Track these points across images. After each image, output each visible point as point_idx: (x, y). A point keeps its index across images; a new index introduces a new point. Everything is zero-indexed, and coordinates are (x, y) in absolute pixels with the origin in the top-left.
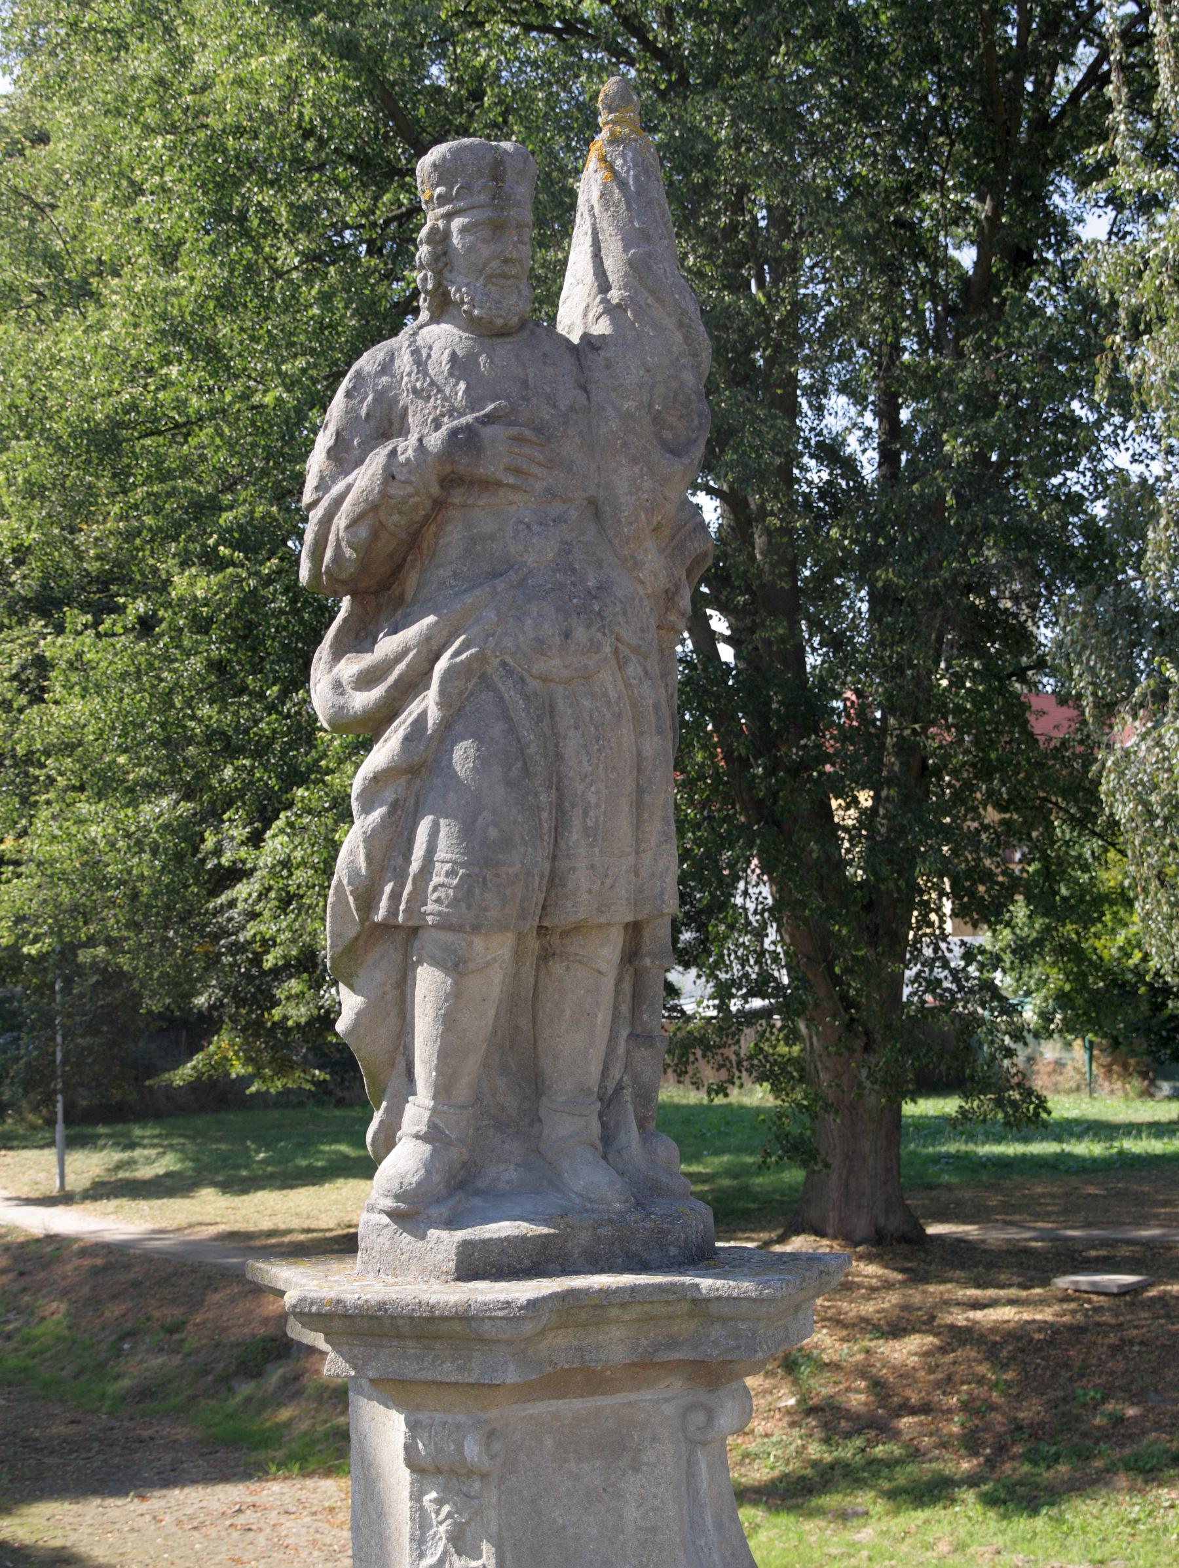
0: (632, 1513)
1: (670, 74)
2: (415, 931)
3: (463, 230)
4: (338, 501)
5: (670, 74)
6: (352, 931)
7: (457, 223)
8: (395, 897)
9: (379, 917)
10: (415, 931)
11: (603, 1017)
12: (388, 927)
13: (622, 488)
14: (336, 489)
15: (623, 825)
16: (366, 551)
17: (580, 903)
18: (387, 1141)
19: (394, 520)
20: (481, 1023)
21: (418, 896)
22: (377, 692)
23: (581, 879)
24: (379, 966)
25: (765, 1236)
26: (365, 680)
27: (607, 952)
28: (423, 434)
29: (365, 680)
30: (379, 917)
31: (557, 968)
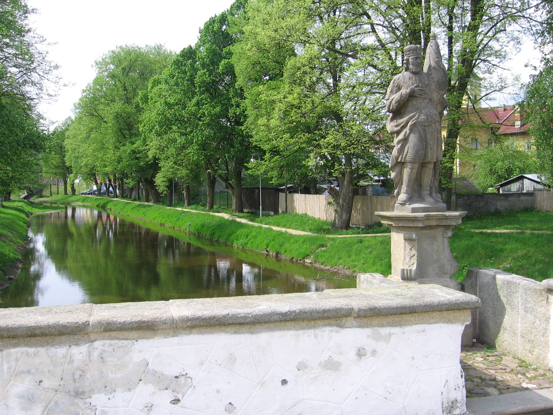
0: (435, 247)
1: (18, 268)
2: (404, 163)
3: (412, 59)
4: (393, 100)
5: (18, 268)
6: (395, 163)
7: (410, 58)
8: (402, 158)
9: (399, 161)
10: (404, 163)
11: (431, 176)
12: (400, 162)
13: (435, 97)
14: (391, 98)
15: (435, 148)
16: (397, 107)
17: (429, 159)
18: (398, 194)
19: (401, 102)
20: (414, 176)
21: (405, 158)
22: (399, 128)
23: (429, 155)
24: (397, 169)
25: (486, 371)
26: (397, 126)
27: (431, 166)
28: (404, 91)
29: (397, 126)
30: (399, 161)
31: (424, 168)
